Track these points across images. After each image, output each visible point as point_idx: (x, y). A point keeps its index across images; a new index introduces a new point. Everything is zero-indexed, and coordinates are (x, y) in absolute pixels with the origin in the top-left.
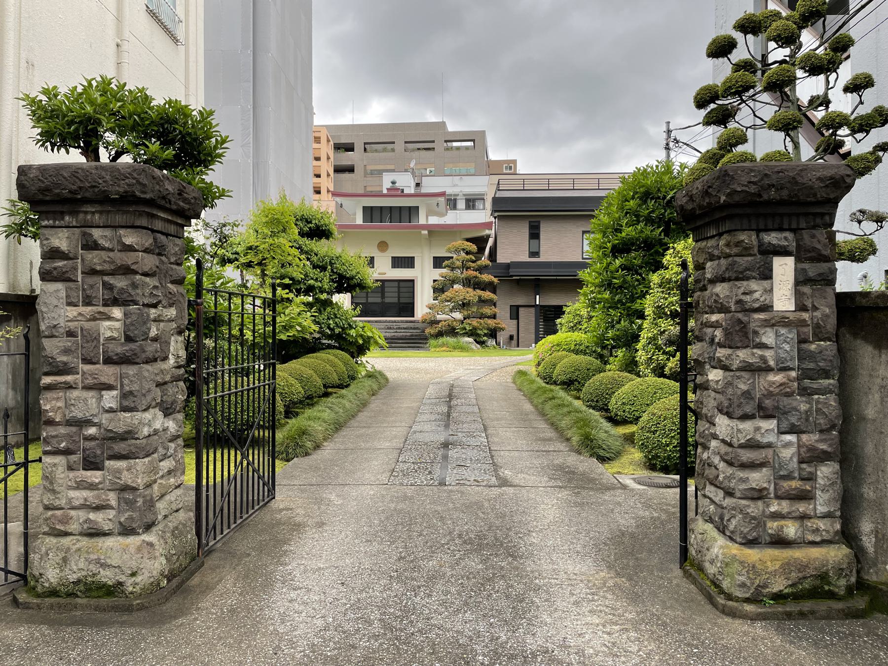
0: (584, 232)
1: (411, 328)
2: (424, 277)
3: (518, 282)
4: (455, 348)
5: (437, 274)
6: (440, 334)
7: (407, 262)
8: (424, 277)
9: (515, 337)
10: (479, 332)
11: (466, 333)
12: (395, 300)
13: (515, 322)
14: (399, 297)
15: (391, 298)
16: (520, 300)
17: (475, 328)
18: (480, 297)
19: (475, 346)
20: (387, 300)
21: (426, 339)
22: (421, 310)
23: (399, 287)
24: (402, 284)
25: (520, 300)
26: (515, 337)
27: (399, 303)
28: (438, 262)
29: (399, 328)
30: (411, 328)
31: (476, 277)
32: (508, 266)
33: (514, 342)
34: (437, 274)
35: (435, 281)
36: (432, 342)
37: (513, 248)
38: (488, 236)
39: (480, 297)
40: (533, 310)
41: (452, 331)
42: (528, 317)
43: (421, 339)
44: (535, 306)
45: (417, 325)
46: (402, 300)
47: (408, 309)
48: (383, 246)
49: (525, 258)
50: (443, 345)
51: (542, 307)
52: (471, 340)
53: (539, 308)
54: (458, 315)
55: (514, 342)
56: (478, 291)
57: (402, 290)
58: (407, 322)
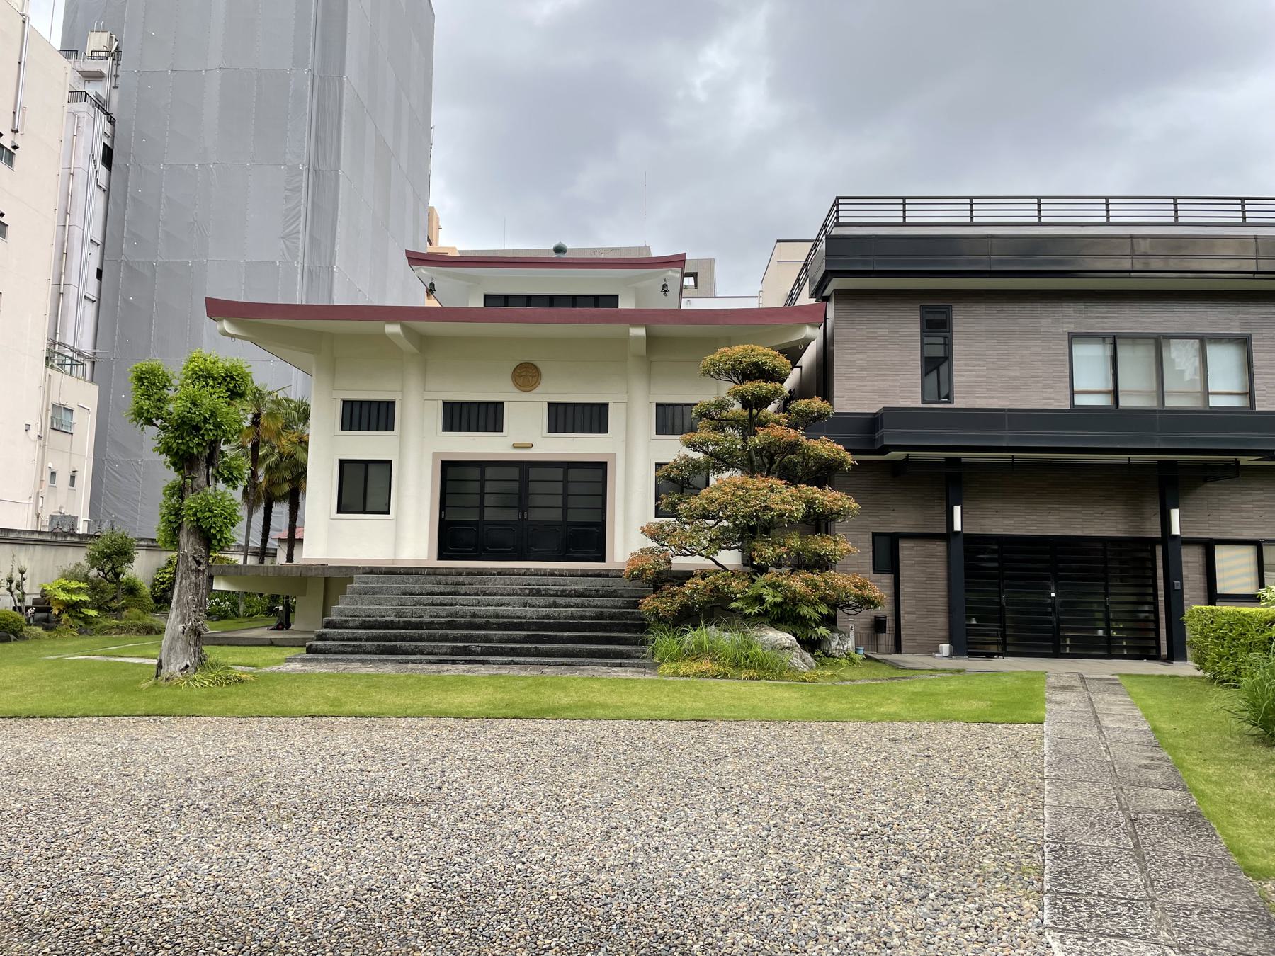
0: (1073, 338)
1: (597, 594)
2: (634, 457)
3: (896, 469)
4: (737, 664)
5: (673, 449)
6: (687, 617)
7: (592, 418)
8: (634, 457)
9: (890, 625)
10: (806, 611)
11: (765, 614)
12: (556, 516)
13: (887, 579)
14: (565, 508)
15: (546, 510)
16: (900, 520)
17: (794, 600)
18: (810, 504)
19: (799, 659)
20: (536, 516)
21: (643, 627)
22: (629, 532)
23: (566, 482)
24: (573, 474)
25: (900, 520)
26: (890, 625)
27: (566, 524)
28: (669, 419)
29: (563, 594)
30: (597, 594)
31: (793, 447)
32: (873, 422)
33: (887, 638)
34: (673, 449)
35: (659, 465)
36: (665, 641)
37: (878, 374)
38: (806, 342)
39: (810, 504)
40: (939, 548)
41: (715, 608)
42: (925, 570)
43: (625, 628)
44: (949, 535)
45: (613, 585)
46: (574, 517)
47: (588, 538)
48: (526, 376)
49: (912, 399)
50: (698, 653)
51: (974, 544)
52: (784, 637)
53: (959, 546)
54: (730, 558)
55: (887, 638)
56: (803, 487)
57: (573, 489)
58: (585, 574)
